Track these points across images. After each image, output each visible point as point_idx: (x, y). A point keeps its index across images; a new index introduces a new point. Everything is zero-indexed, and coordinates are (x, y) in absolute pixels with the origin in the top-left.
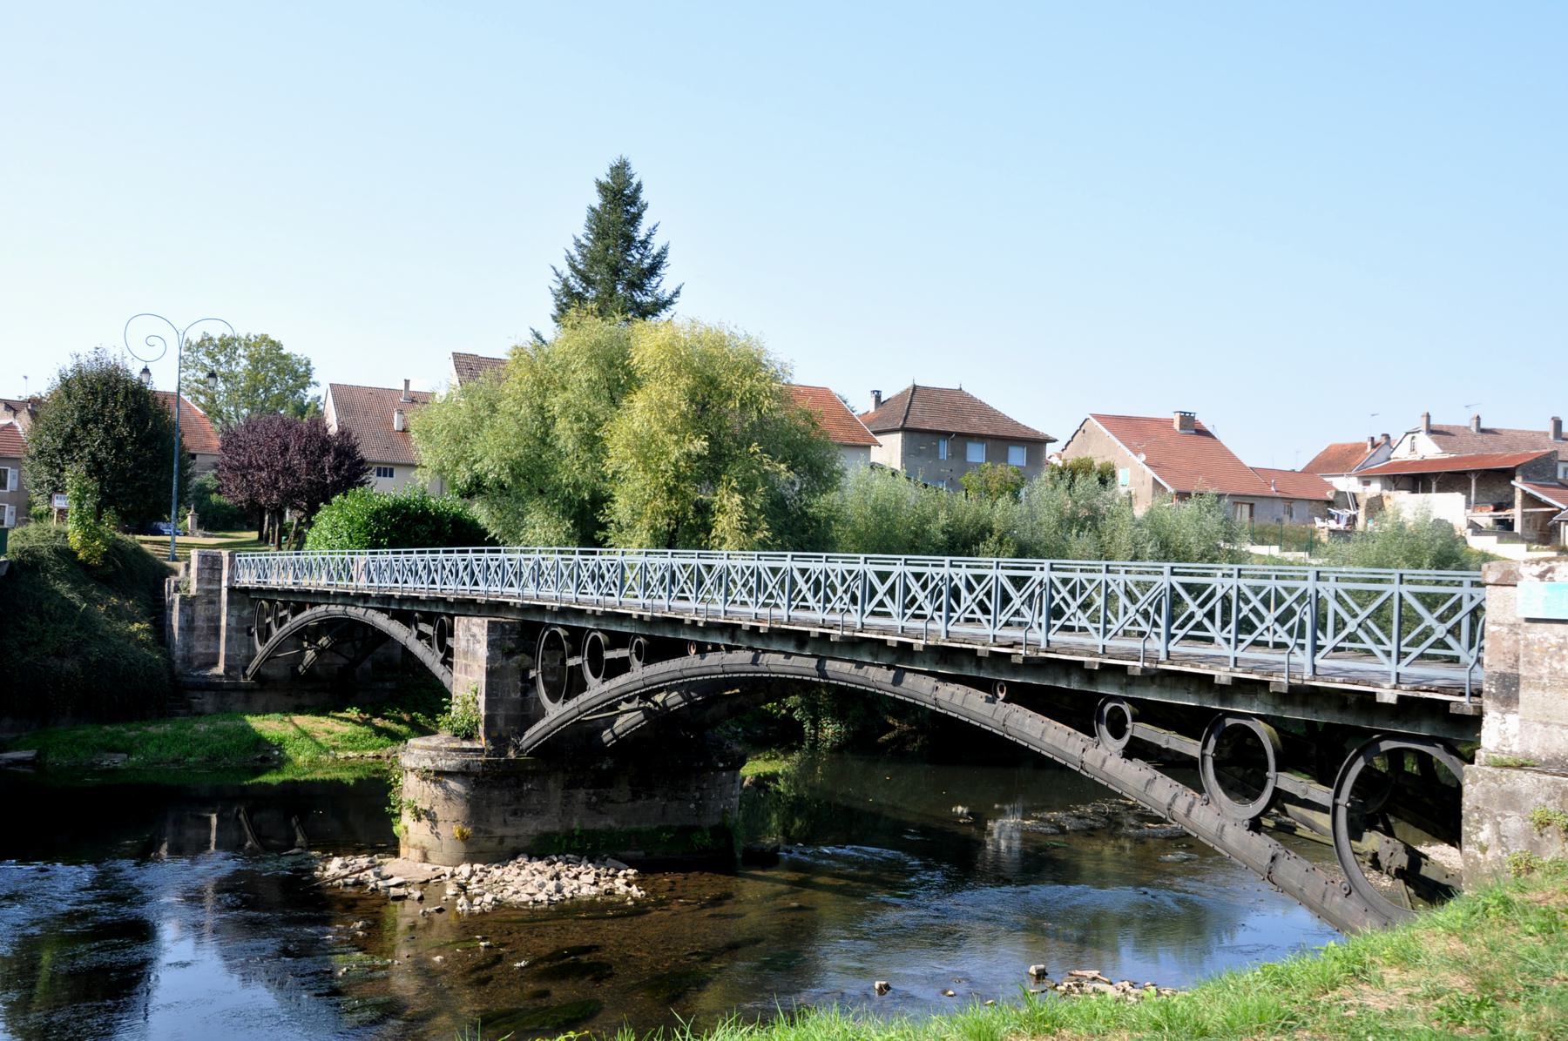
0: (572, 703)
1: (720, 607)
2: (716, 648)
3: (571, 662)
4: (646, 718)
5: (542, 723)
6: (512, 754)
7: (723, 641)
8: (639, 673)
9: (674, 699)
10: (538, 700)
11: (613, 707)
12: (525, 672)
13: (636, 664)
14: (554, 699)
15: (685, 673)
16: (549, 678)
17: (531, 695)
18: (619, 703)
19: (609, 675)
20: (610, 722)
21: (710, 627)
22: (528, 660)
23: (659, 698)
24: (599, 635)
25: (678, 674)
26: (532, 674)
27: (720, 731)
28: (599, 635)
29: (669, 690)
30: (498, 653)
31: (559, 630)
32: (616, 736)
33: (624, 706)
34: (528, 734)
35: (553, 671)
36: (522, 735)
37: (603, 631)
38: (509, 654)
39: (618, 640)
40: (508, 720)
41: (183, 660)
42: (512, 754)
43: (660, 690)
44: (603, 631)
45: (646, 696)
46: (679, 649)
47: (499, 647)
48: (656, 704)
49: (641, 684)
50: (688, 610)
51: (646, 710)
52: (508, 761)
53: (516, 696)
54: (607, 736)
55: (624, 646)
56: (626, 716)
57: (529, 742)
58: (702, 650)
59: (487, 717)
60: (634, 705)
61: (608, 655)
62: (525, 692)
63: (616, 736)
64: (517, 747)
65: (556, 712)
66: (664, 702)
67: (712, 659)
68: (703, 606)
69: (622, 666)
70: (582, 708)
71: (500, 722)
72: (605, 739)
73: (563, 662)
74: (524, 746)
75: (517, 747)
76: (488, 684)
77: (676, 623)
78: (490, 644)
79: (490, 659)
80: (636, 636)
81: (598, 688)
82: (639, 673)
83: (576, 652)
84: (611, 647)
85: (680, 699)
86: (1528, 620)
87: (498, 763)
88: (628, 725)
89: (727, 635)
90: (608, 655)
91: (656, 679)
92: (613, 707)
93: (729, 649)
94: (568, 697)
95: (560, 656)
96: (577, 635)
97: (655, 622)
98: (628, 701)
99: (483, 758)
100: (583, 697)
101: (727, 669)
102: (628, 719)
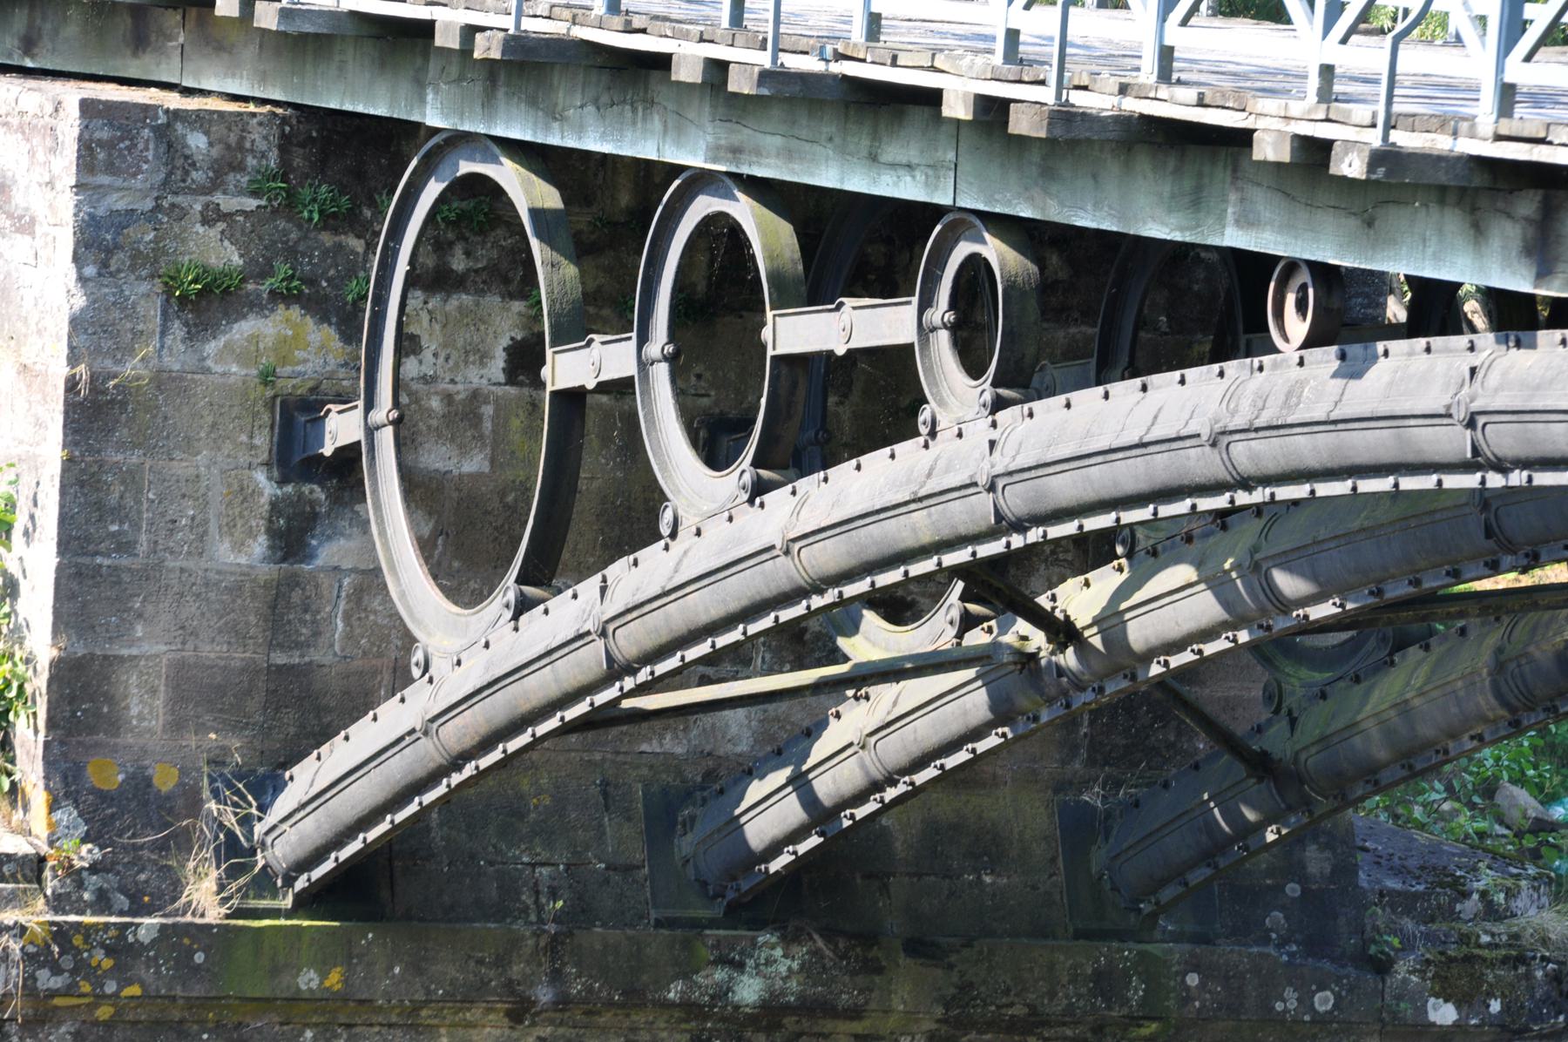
0: (571, 610)
1: (1476, 63)
2: (1435, 310)
3: (568, 368)
4: (1002, 713)
5: (393, 717)
6: (204, 896)
7: (1480, 266)
8: (974, 449)
9: (1174, 609)
10: (371, 580)
11: (806, 642)
12: (297, 414)
13: (953, 391)
14: (463, 575)
15: (1247, 455)
16: (437, 458)
17: (331, 552)
18: (844, 618)
19: (798, 450)
20: (788, 733)
21: (1401, 183)
22: (313, 346)
23: (1081, 599)
24: (743, 210)
25: (1200, 463)
26: (341, 428)
27: (1438, 813)
28: (743, 210)
29: (1145, 551)
30: (145, 297)
31: (509, 175)
32: (820, 815)
33: (874, 640)
34: (305, 778)
35: (464, 416)
36: (267, 785)
37: (761, 189)
38: (206, 303)
39: (860, 246)
40: (194, 693)
41: (116, 745)
42: (204, 896)
43: (1090, 552)
44: (761, 189)
45: (1001, 585)
46: (1218, 309)
47: (147, 261)
48: (1063, 632)
49: (979, 509)
50: (1276, 83)
51: (1013, 678)
52: (182, 939)
53: (245, 553)
54: (768, 814)
55: (884, 281)
56: (886, 698)
57: (311, 829)
58: (1348, 316)
59: (65, 674)
60: (933, 632)
61: (795, 332)
62: (292, 536)
63: (820, 815)
64: (235, 854)
65: (474, 659)
66: (1112, 620)
67: (1413, 377)
68: (1368, 55)
69: (870, 403)
70: (629, 641)
71: (144, 707)
72: (759, 830)
73: (525, 361)
74: (281, 851)
75: (235, 854)
76: (80, 481)
77: (1201, 150)
78: (98, 245)
79: (92, 332)
80: (963, 222)
81: (721, 529)
82: (974, 449)
83: (606, 308)
84: (817, 286)
85: (1204, 607)
86: (806, 53)
87: (122, 948)
88: (895, 748)
89: (1507, 233)
90: (795, 332)
91: (1065, 487)
92: (806, 642)
93: (1514, 316)
94: (545, 572)
95: (504, 324)
96: (612, 209)
97: (1075, 141)
98: (899, 607)
99: (36, 915)
100: (632, 577)
101: (1502, 439)
102: (898, 718)
